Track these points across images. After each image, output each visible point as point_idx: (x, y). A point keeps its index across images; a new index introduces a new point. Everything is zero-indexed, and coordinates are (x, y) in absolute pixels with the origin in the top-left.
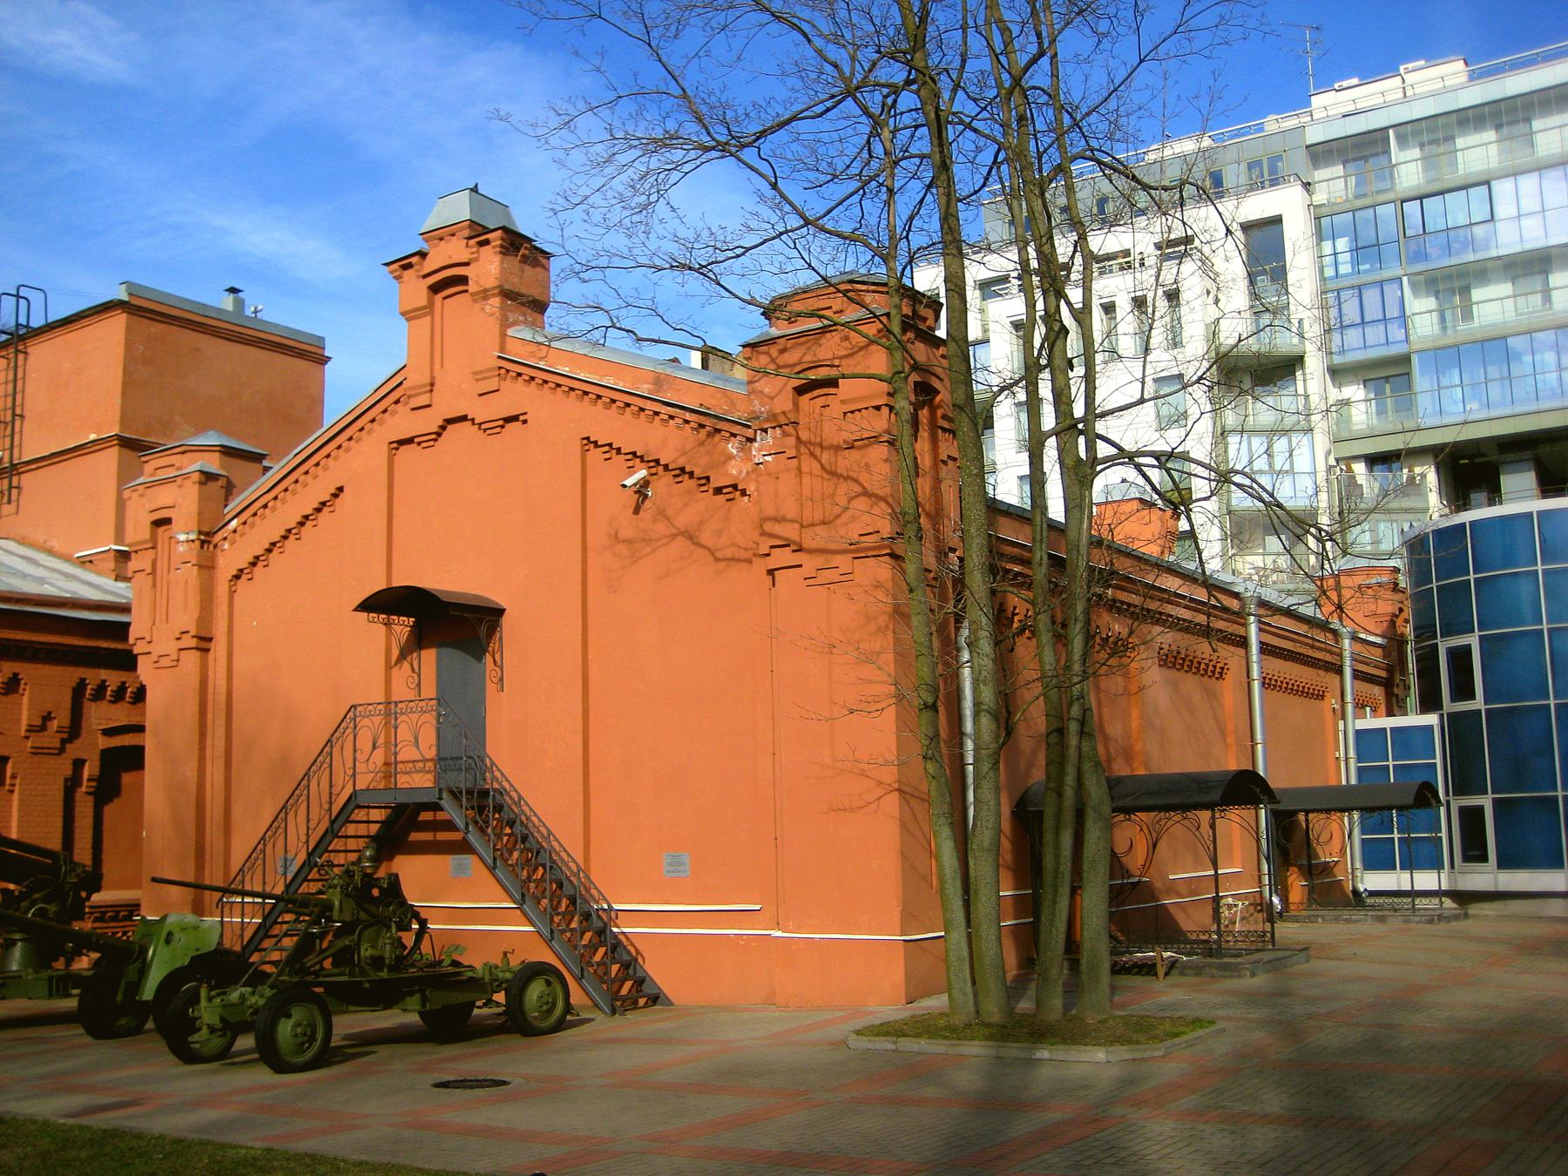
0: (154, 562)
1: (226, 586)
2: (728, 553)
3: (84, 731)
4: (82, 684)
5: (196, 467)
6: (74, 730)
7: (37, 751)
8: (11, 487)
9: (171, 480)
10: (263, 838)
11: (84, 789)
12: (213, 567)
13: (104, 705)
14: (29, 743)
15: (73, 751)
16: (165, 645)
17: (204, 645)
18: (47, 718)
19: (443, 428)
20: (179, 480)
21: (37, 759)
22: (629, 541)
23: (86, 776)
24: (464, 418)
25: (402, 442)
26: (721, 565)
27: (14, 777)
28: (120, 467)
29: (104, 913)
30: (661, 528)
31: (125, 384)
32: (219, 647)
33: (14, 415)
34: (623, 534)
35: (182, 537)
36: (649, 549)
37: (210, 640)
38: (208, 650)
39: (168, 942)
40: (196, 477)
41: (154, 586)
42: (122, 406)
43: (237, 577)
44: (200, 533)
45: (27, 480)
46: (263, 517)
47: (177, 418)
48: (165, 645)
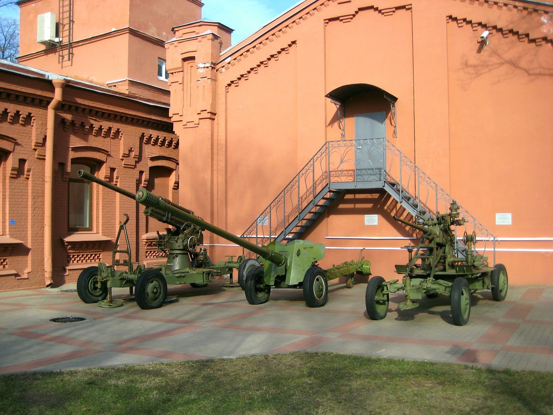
0: (183, 77)
1: (224, 89)
2: (537, 71)
3: (143, 158)
4: (143, 135)
5: (209, 32)
6: (139, 158)
7: (127, 166)
8: (69, 53)
9: (195, 38)
10: (270, 205)
11: (142, 185)
12: (216, 80)
13: (150, 146)
14: (123, 162)
15: (140, 167)
16: (190, 116)
17: (213, 117)
18: (130, 151)
19: (357, 12)
20: (199, 38)
21: (126, 170)
22: (474, 66)
23: (143, 179)
24: (371, 7)
25: (331, 20)
26: (533, 77)
27: (117, 178)
28: (129, 43)
29: (151, 242)
30: (495, 60)
31: (131, 5)
32: (220, 118)
33: (70, 20)
34: (471, 62)
35: (202, 65)
36: (486, 70)
37: (215, 114)
38: (214, 119)
39: (298, 255)
40: (211, 36)
41: (183, 89)
42: (130, 16)
43: (229, 85)
44: (212, 63)
45: (75, 50)
46: (246, 56)
47: (150, 24)
48: (190, 116)
